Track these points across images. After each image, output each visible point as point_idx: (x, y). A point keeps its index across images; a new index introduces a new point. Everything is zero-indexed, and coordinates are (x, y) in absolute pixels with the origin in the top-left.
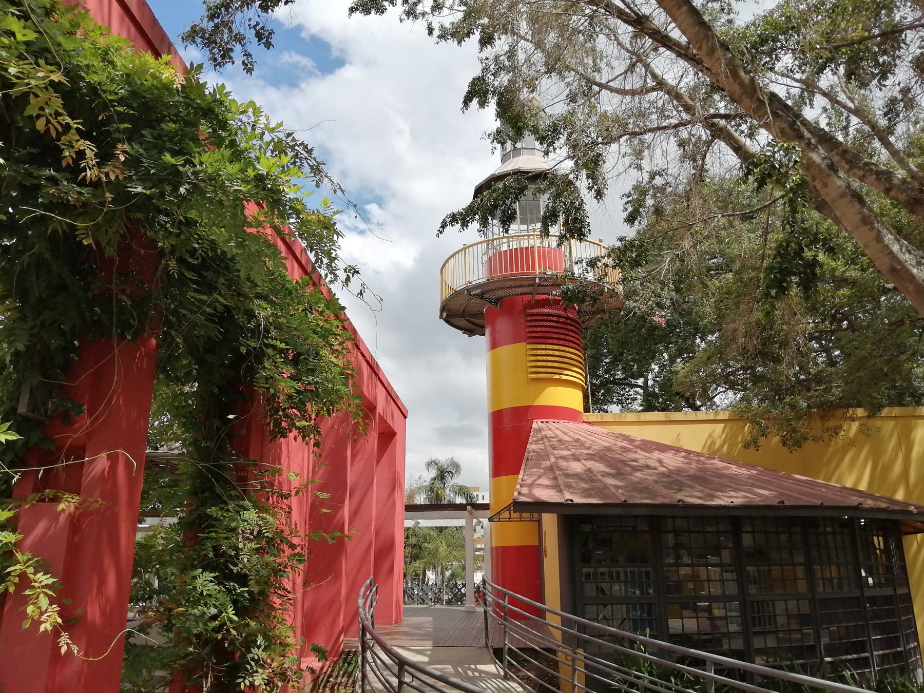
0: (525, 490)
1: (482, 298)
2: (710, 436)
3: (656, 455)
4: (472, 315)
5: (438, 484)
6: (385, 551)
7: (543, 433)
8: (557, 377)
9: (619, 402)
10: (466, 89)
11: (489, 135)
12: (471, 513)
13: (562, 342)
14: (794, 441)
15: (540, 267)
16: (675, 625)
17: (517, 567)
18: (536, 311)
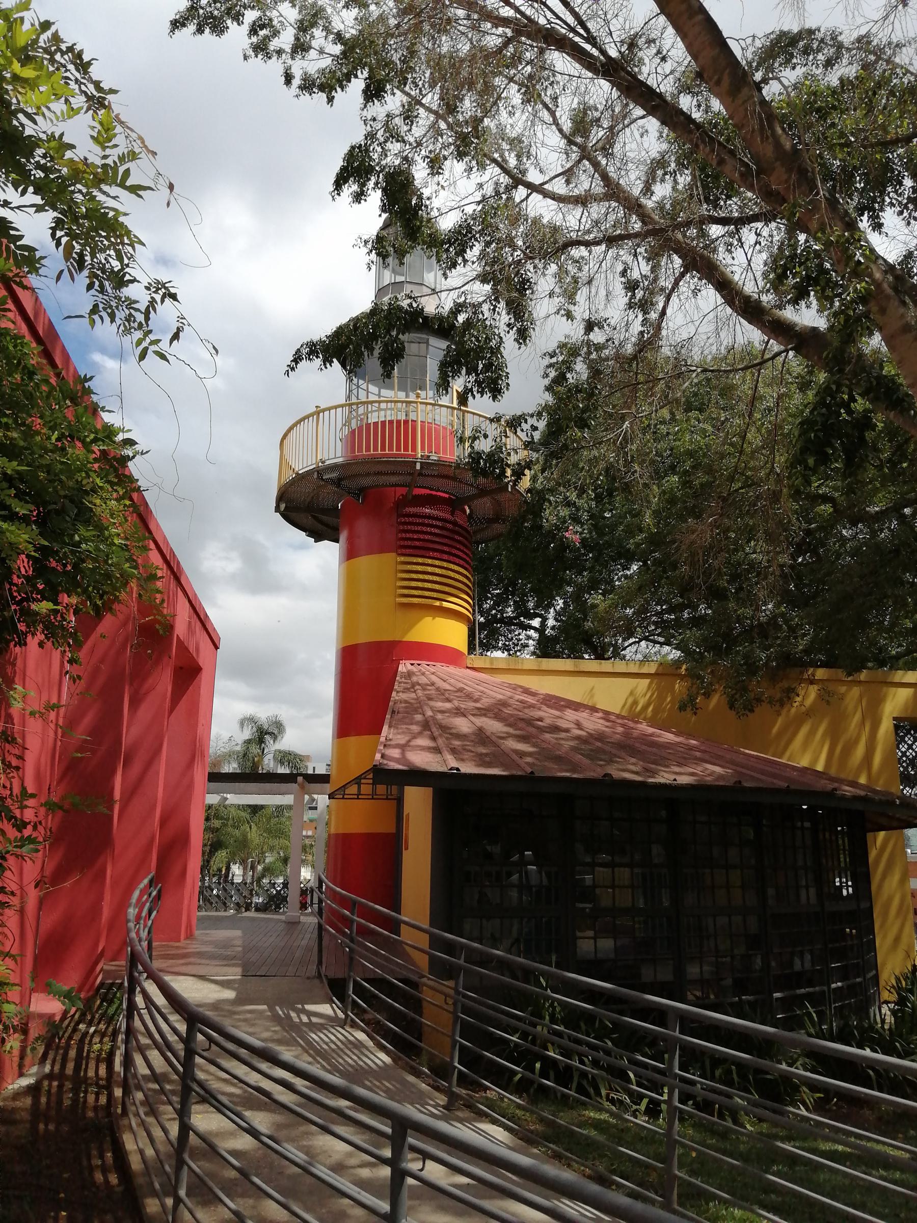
0: (395, 753)
1: (338, 486)
2: (631, 693)
3: (570, 714)
4: (325, 511)
5: (255, 750)
6: (174, 845)
7: (414, 679)
8: (437, 603)
9: (506, 648)
10: (338, 163)
11: (366, 242)
12: (302, 787)
13: (445, 557)
14: (742, 702)
15: (423, 449)
16: (586, 946)
17: (365, 862)
18: (412, 510)
